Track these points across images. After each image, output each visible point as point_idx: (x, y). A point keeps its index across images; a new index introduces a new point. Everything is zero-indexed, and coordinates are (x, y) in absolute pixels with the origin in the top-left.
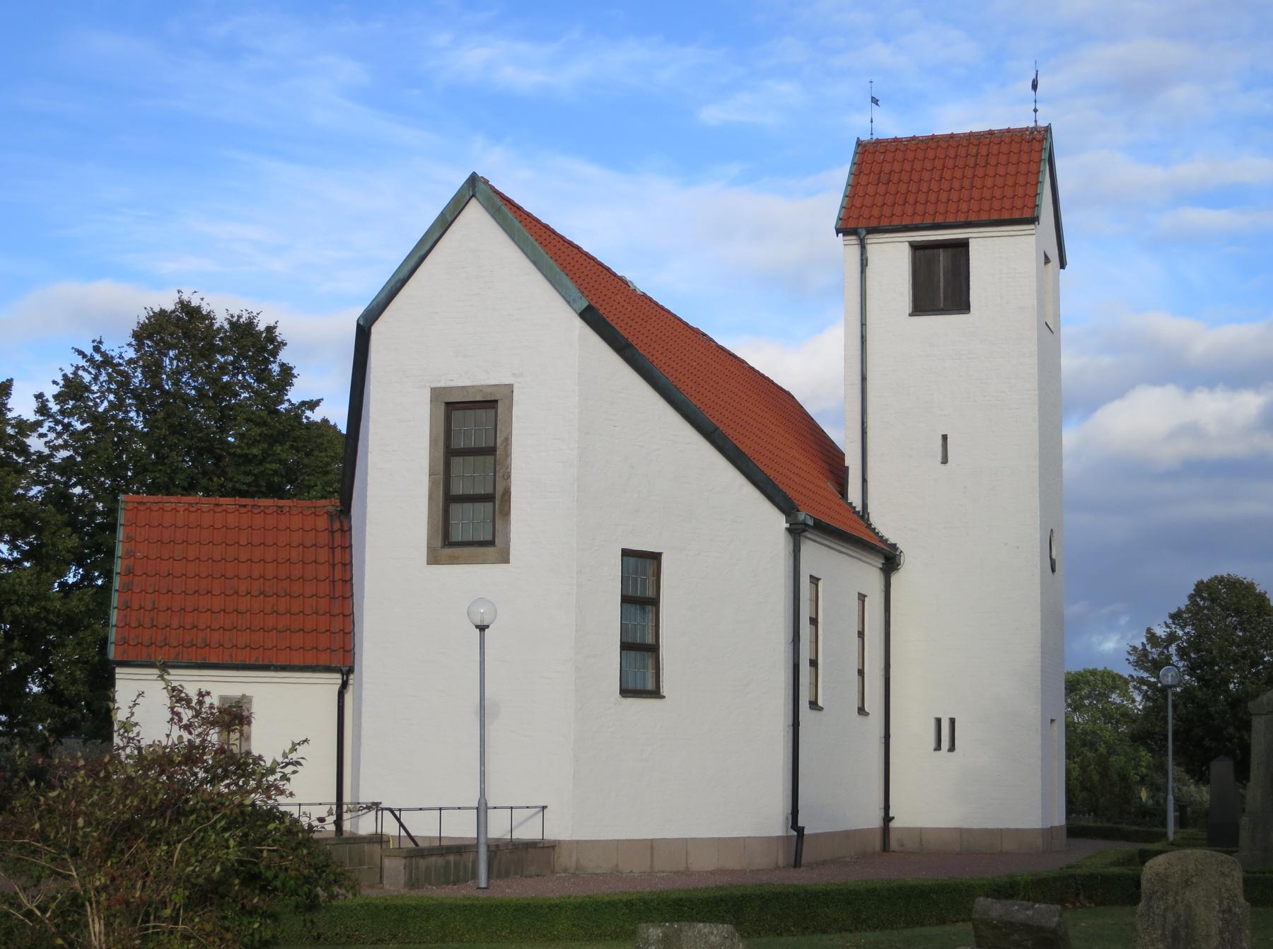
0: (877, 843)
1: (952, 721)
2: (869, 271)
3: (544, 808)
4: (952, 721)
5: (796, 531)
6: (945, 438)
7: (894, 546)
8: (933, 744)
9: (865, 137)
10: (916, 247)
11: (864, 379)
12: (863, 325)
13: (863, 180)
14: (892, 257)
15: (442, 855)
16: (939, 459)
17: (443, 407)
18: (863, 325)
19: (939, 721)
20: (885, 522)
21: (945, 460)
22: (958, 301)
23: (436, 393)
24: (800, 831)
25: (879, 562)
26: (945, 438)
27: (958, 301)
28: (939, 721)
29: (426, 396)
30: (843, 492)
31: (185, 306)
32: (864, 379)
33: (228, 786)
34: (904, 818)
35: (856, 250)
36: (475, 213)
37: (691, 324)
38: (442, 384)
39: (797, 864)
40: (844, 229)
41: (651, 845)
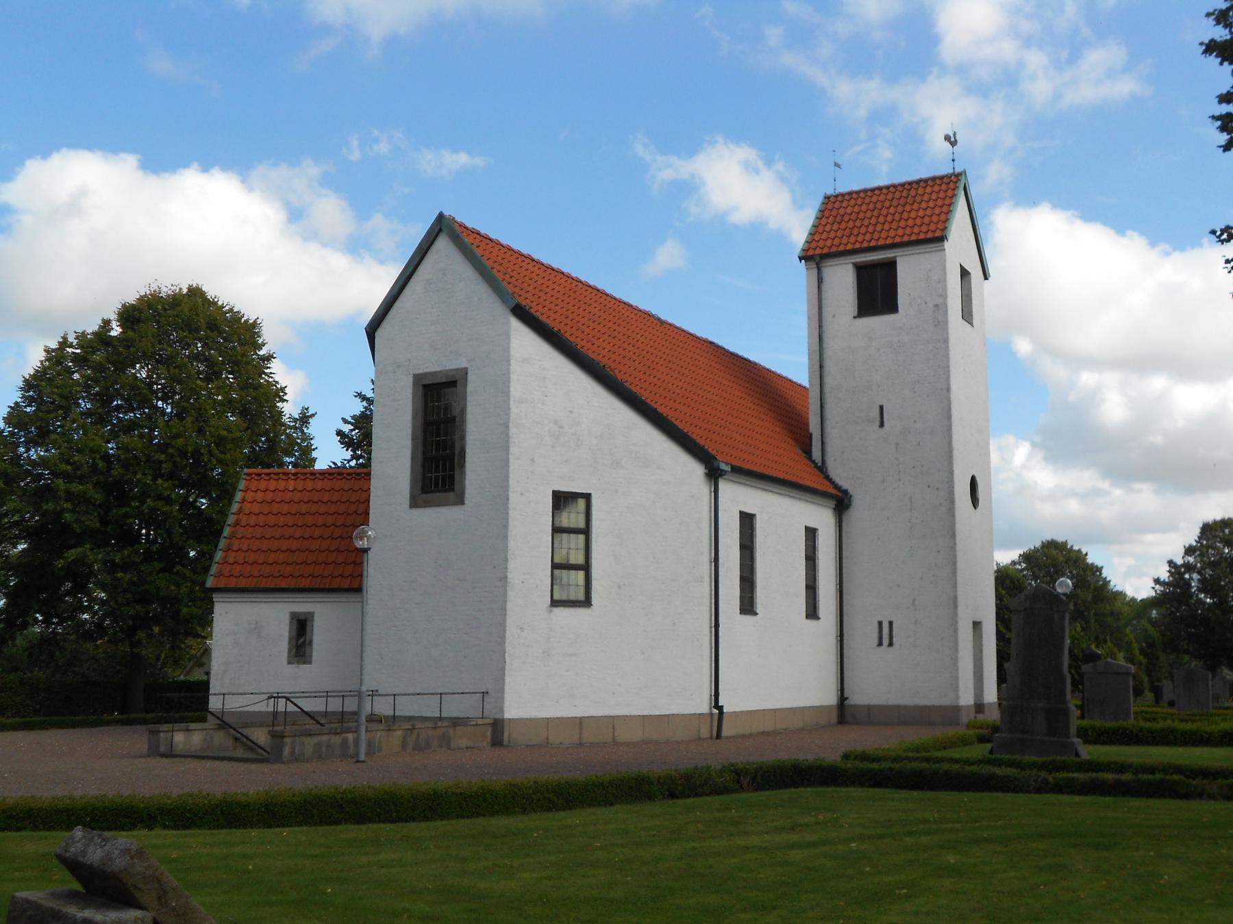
0: (834, 717)
1: (891, 623)
2: (824, 287)
3: (485, 694)
4: (891, 623)
5: (714, 475)
6: (881, 408)
7: (845, 492)
8: (876, 641)
9: (830, 192)
10: (860, 269)
11: (821, 367)
12: (820, 327)
13: (824, 221)
14: (842, 279)
15: (336, 734)
16: (878, 423)
17: (421, 388)
18: (820, 327)
19: (880, 623)
20: (840, 473)
21: (882, 425)
22: (890, 306)
23: (417, 378)
24: (720, 708)
25: (832, 504)
26: (881, 408)
27: (890, 306)
28: (880, 623)
29: (411, 379)
30: (808, 453)
31: (255, 325)
32: (821, 367)
33: (1114, 657)
34: (730, 703)
35: (815, 271)
36: (443, 244)
37: (699, 334)
38: (421, 371)
39: (719, 736)
40: (805, 257)
41: (580, 722)
